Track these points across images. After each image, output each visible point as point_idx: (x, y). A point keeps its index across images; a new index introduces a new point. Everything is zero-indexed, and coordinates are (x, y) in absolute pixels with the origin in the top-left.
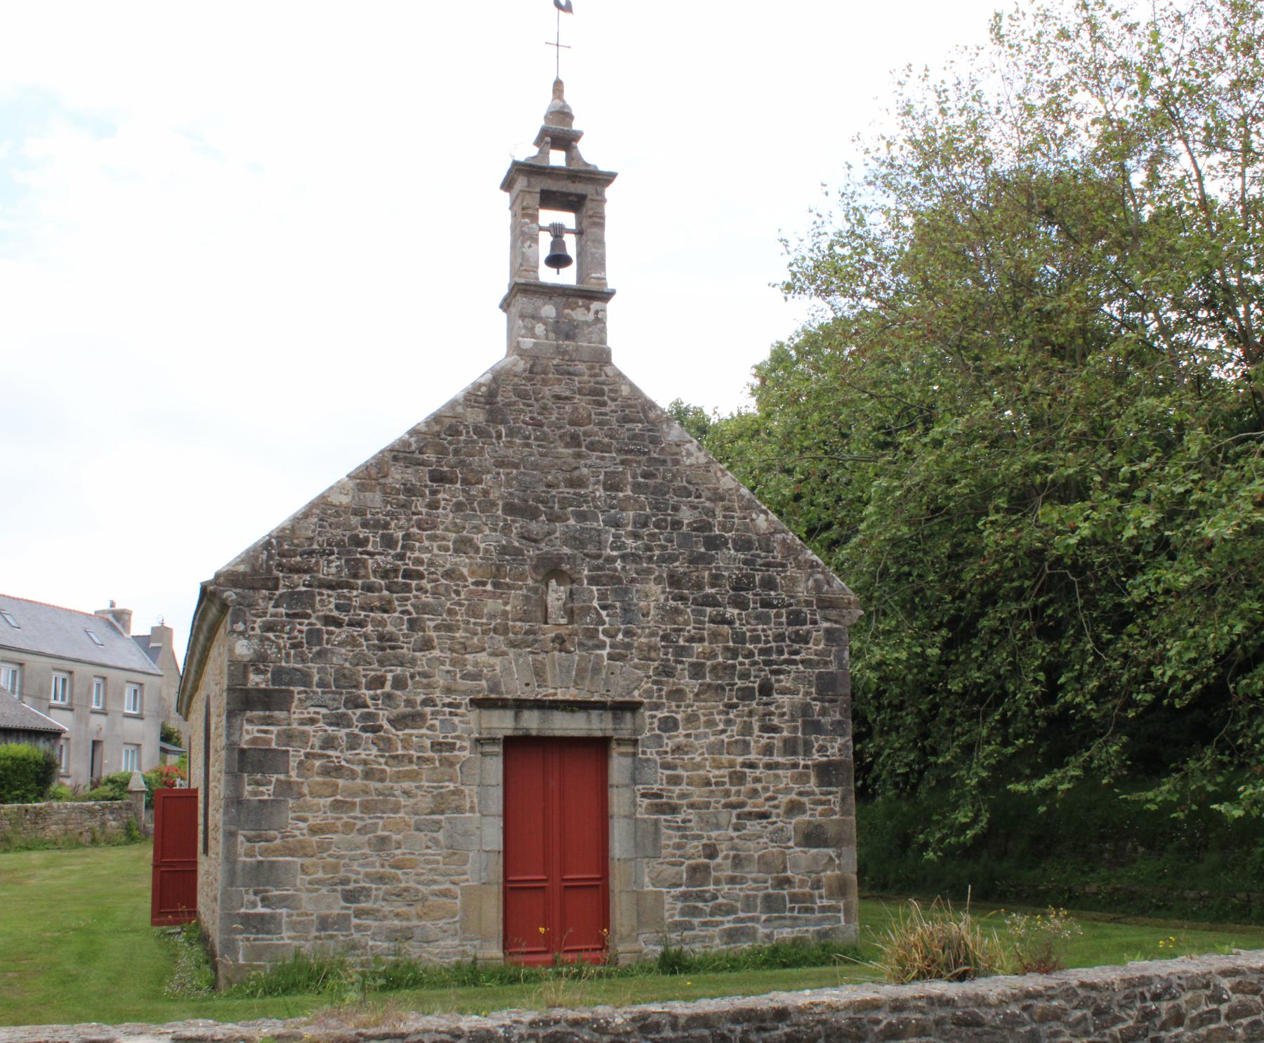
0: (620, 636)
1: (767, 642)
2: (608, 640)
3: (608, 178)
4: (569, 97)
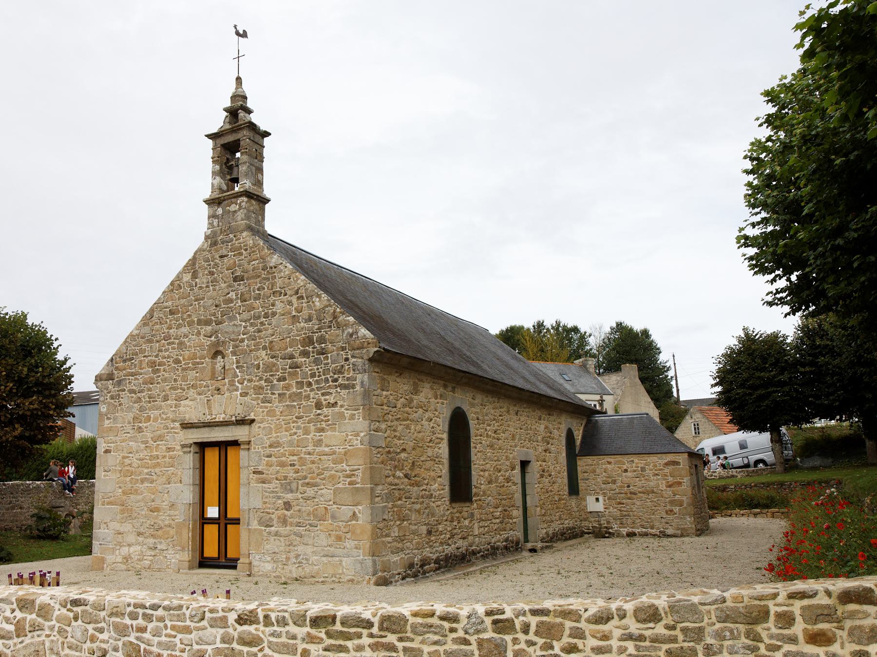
0: (246, 382)
1: (319, 376)
2: (240, 386)
3: (267, 134)
4: (247, 88)
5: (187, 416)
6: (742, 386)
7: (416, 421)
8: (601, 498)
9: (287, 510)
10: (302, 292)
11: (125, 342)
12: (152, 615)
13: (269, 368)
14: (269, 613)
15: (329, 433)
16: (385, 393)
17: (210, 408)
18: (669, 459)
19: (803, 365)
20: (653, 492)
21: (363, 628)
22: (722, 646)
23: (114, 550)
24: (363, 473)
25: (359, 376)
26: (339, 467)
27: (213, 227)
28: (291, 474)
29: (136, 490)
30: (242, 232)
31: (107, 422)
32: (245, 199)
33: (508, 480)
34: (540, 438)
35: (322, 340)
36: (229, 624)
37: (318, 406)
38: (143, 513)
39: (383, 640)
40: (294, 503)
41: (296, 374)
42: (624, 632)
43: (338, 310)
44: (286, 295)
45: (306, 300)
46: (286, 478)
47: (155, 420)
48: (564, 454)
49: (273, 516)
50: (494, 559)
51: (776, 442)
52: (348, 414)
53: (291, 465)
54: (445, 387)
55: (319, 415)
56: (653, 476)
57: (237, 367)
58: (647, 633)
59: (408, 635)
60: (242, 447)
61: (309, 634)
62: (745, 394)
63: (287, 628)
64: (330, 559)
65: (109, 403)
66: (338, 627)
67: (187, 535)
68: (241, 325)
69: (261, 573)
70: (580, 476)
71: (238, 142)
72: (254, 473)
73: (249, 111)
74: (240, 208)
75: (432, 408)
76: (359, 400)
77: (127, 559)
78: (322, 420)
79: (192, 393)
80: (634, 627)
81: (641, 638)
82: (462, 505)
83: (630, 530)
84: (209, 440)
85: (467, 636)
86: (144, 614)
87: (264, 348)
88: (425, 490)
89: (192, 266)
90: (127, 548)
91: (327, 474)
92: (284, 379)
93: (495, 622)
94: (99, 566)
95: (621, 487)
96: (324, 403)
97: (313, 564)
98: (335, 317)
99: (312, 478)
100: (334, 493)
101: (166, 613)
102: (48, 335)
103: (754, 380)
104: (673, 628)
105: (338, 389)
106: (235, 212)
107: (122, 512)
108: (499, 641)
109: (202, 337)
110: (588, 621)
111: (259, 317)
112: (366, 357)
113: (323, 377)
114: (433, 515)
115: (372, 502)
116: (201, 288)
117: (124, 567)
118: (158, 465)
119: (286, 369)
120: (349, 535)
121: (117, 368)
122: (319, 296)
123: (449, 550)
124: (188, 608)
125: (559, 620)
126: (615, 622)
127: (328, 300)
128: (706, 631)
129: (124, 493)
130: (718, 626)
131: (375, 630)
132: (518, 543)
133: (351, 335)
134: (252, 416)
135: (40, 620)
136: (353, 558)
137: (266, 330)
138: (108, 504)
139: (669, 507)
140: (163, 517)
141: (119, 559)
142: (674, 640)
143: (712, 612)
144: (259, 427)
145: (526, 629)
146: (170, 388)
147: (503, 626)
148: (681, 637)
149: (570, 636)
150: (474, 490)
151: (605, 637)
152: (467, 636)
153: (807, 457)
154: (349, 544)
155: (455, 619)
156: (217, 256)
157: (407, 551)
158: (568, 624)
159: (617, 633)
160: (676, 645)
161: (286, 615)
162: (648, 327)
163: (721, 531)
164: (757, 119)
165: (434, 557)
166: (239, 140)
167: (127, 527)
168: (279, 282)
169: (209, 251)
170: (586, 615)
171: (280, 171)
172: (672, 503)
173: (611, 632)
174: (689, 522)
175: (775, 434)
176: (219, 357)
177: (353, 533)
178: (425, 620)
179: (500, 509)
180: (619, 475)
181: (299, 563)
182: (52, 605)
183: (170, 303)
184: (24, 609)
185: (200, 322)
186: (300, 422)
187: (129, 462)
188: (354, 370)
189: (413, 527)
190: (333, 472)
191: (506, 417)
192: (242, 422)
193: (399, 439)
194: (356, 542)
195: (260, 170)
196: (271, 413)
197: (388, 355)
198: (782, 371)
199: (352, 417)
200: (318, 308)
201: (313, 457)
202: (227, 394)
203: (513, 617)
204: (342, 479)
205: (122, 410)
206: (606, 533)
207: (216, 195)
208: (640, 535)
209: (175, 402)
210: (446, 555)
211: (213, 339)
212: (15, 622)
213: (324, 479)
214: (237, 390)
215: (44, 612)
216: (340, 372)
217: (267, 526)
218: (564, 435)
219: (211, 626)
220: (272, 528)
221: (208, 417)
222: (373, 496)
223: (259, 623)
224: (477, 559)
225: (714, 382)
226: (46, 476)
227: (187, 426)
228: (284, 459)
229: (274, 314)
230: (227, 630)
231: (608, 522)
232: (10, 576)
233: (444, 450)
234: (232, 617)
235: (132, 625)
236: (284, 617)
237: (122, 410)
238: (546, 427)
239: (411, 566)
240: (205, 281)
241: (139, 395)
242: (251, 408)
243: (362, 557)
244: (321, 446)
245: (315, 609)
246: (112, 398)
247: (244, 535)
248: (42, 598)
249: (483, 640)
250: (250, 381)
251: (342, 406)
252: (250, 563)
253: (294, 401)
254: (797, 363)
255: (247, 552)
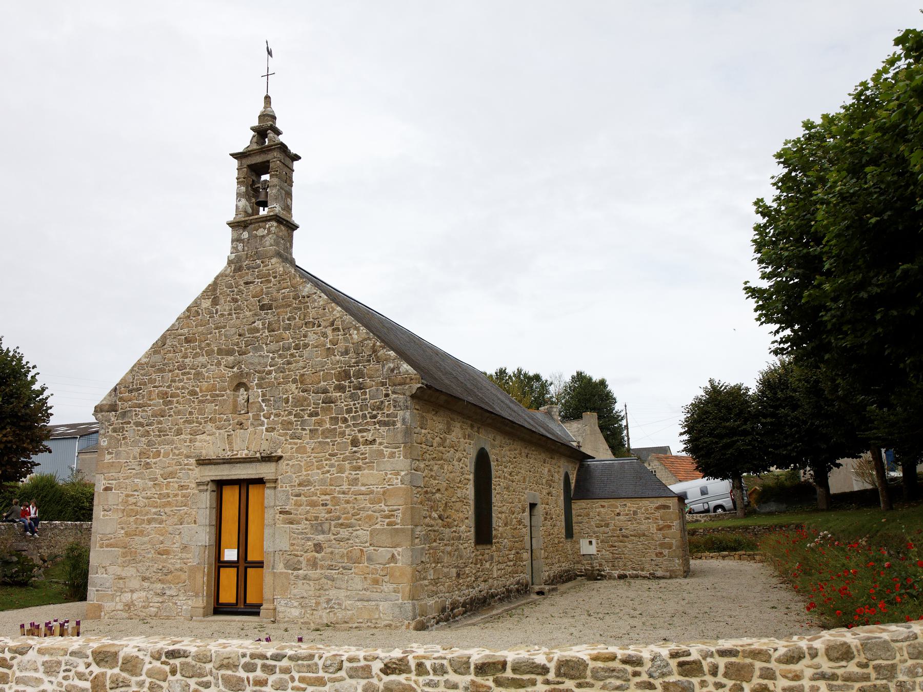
0: (272, 417)
1: (356, 412)
2: (266, 421)
3: (297, 158)
4: (275, 108)
5: (204, 452)
6: (711, 434)
7: (449, 461)
8: (594, 541)
9: (317, 552)
10: (338, 323)
11: (132, 370)
12: (275, 666)
13: (299, 402)
14: (423, 661)
15: (366, 471)
16: (423, 431)
17: (230, 443)
18: (659, 503)
19: (765, 417)
20: (644, 535)
21: (538, 674)
22: (914, 682)
23: (113, 597)
24: (403, 514)
25: (400, 413)
26: (377, 507)
27: (237, 251)
28: (323, 515)
29: (142, 532)
30: (271, 258)
31: (108, 457)
32: (275, 224)
33: (520, 522)
34: (544, 481)
35: (360, 374)
36: (373, 673)
37: (355, 443)
38: (150, 556)
39: (561, 687)
40: (326, 545)
41: (330, 409)
42: (816, 671)
43: (378, 344)
44: (319, 326)
45: (342, 332)
46: (316, 518)
47: (166, 455)
48: (562, 498)
49: (301, 559)
50: (510, 602)
51: (738, 488)
52: (387, 452)
53: (323, 505)
54: (472, 427)
55: (355, 452)
56: (637, 517)
57: (263, 401)
58: (839, 672)
59: (588, 680)
60: (268, 485)
61: (473, 682)
62: (712, 443)
63: (446, 677)
64: (366, 603)
65: (111, 437)
66: (509, 674)
67: (202, 580)
68: (268, 356)
69: (286, 619)
70: (574, 519)
71: (265, 164)
72: (280, 513)
73: (278, 133)
74: (268, 234)
75: (462, 448)
76: (400, 437)
77: (128, 606)
78: (359, 458)
79: (210, 427)
80: (826, 666)
81: (834, 677)
82: (485, 547)
83: (622, 572)
84: (229, 478)
85: (651, 680)
86: (264, 666)
87: (295, 381)
88: (455, 532)
89: (212, 292)
90: (129, 594)
91: (363, 514)
92: (317, 414)
93: (681, 664)
94: (96, 613)
95: (613, 530)
96: (361, 440)
97: (346, 609)
98: (375, 351)
99: (346, 519)
100: (371, 534)
101: (292, 664)
102: (24, 362)
103: (722, 428)
104: (866, 666)
105: (377, 426)
106: (263, 236)
107: (124, 555)
108: (686, 684)
109: (222, 368)
110: (779, 661)
111: (289, 349)
112: (408, 393)
113: (360, 413)
114: (461, 557)
115: (413, 544)
116: (222, 315)
117: (125, 615)
118: (169, 504)
119: (319, 404)
120: (386, 579)
121: (121, 399)
122: (357, 329)
123: (473, 593)
124: (321, 657)
125: (748, 661)
126: (806, 661)
127: (367, 333)
128: (899, 668)
129: (126, 533)
130: (910, 662)
131: (551, 676)
132: (527, 585)
133: (392, 370)
134: (279, 453)
135: (124, 675)
136: (392, 601)
137: (297, 362)
138: (107, 546)
139: (658, 550)
140: (173, 561)
141: (120, 606)
142: (867, 678)
143: (905, 649)
144: (288, 465)
145: (714, 671)
146: (184, 422)
147: (689, 668)
148: (873, 675)
149: (761, 677)
150: (494, 533)
151: (797, 677)
152: (651, 680)
153: (765, 503)
154: (387, 587)
155: (638, 662)
156: (242, 283)
157: (441, 595)
158: (758, 665)
159: (809, 673)
160: (869, 684)
161: (445, 662)
162: (605, 378)
163: (702, 573)
164: (773, 178)
165: (462, 600)
166: (268, 162)
167: (130, 571)
168: (312, 313)
169: (232, 277)
170: (776, 655)
171: (310, 194)
172: (662, 545)
173: (802, 671)
174: (677, 564)
175: (737, 481)
176: (242, 390)
177: (392, 576)
178: (606, 664)
179: (513, 552)
180: (612, 519)
181: (331, 608)
182: (141, 657)
183: (186, 330)
184: (103, 663)
185: (220, 351)
186: (334, 460)
187: (134, 501)
188: (395, 407)
189: (446, 570)
190: (370, 513)
191: (519, 460)
192: (268, 459)
193: (435, 479)
194: (395, 586)
195: (289, 195)
196: (301, 450)
197: (429, 392)
198: (746, 421)
199: (392, 455)
200: (355, 341)
201: (348, 497)
202: (251, 429)
203: (701, 658)
204: (379, 519)
205: (126, 444)
206: (598, 575)
207: (241, 218)
208: (631, 577)
209: (189, 436)
210: (471, 598)
211: (235, 369)
212: (91, 678)
213: (360, 519)
214: (262, 425)
215: (131, 665)
216: (379, 408)
217: (295, 569)
218: (562, 478)
219: (351, 677)
220: (300, 572)
221: (229, 453)
222: (413, 538)
223: (410, 672)
224: (495, 602)
225: (683, 431)
226: (6, 517)
227: (203, 462)
228: (315, 498)
229: (306, 346)
230: (370, 680)
231: (601, 565)
232: (22, 626)
233: (470, 491)
234: (377, 666)
235: (248, 679)
236: (442, 665)
237: (126, 444)
238: (549, 471)
239: (443, 610)
240: (227, 308)
241: (147, 428)
242: (279, 445)
243: (400, 601)
244: (357, 485)
245: (477, 655)
246: (114, 430)
247: (268, 579)
248: (125, 649)
249: (669, 683)
250: (277, 415)
251: (380, 444)
252: (275, 609)
253: (327, 437)
254: (756, 416)
255: (271, 597)
